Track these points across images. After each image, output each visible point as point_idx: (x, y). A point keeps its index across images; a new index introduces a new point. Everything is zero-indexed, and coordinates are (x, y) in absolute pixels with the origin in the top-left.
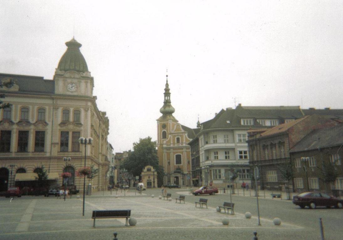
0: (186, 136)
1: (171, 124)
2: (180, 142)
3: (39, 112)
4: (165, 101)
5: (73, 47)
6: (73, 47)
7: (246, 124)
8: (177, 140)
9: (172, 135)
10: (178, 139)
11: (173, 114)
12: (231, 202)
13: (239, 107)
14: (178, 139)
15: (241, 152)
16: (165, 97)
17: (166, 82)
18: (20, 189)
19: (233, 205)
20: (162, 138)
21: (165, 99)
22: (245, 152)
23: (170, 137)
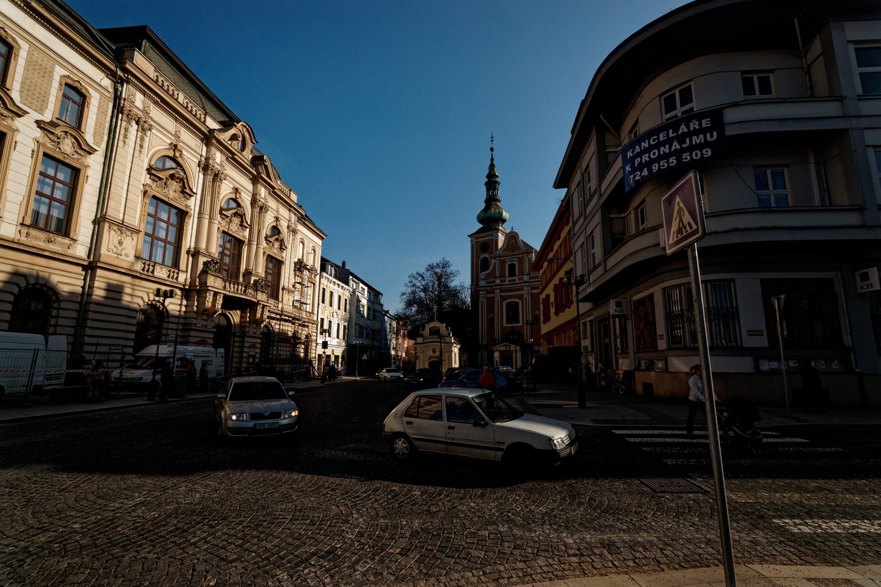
10: (512, 268)
14: (512, 268)
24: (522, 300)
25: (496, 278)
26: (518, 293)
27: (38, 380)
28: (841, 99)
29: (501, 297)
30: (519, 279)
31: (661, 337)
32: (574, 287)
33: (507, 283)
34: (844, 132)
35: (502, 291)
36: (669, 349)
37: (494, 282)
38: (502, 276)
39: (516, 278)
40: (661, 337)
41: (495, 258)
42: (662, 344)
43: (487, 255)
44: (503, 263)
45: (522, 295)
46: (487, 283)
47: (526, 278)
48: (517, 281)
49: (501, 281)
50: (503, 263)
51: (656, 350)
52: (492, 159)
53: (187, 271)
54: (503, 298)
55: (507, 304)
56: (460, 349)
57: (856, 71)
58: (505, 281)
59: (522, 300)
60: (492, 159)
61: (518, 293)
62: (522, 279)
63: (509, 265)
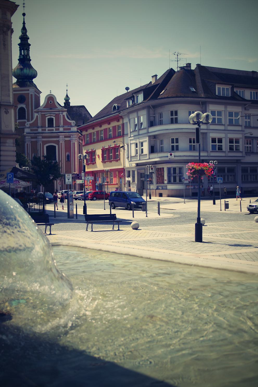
0: (64, 116)
1: (33, 96)
2: (54, 126)
3: (162, 124)
4: (22, 57)
5: (19, 5)
6: (19, 5)
7: (253, 99)
8: (251, 141)
9: (40, 113)
10: (51, 121)
11: (34, 80)
12: (85, 202)
13: (12, 23)
14: (51, 121)
15: (214, 140)
16: (20, 50)
17: (23, 20)
18: (210, 191)
19: (215, 204)
20: (17, 119)
21: (21, 54)
22: (237, 141)
23: (37, 116)
24: (59, 145)
25: (38, 127)
26: (55, 139)
27: (15, 145)
28: (207, 152)
29: (43, 142)
30: (56, 130)
31: (166, 180)
32: (252, 176)
33: (47, 131)
34: (206, 133)
35: (43, 137)
36: (168, 183)
37: (37, 130)
38: (43, 126)
39: (54, 129)
40: (166, 180)
41: (37, 112)
42: (166, 182)
43: (24, 106)
44: (43, 117)
45: (58, 141)
46: (31, 130)
47: (61, 129)
48: (54, 131)
49: (42, 130)
50: (43, 117)
51: (164, 183)
52: (24, 23)
53: (130, 144)
54: (44, 143)
55: (47, 147)
56: (19, 165)
57: (211, 144)
58: (45, 130)
59: (59, 145)
60: (24, 23)
61: (55, 139)
62: (59, 129)
63: (48, 119)
